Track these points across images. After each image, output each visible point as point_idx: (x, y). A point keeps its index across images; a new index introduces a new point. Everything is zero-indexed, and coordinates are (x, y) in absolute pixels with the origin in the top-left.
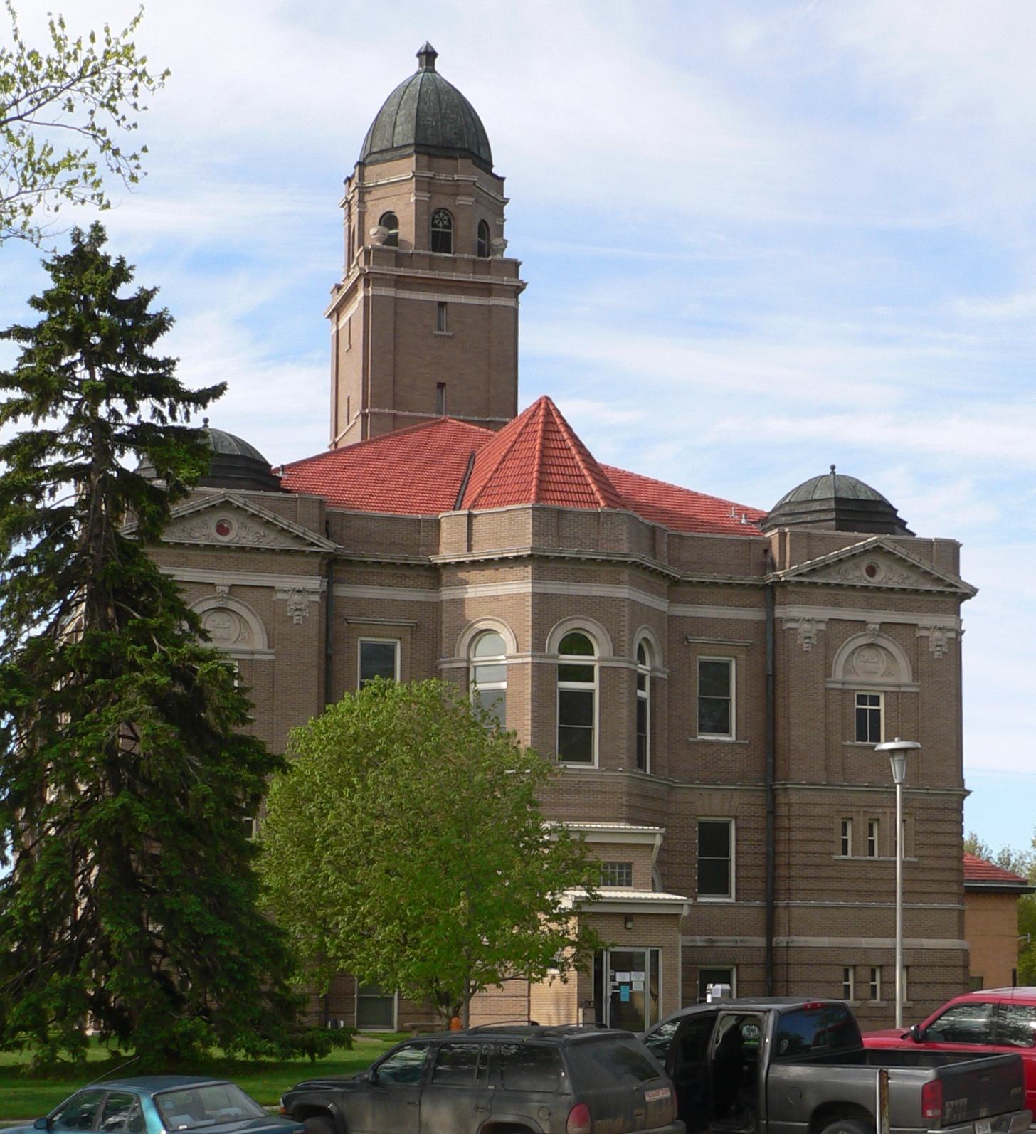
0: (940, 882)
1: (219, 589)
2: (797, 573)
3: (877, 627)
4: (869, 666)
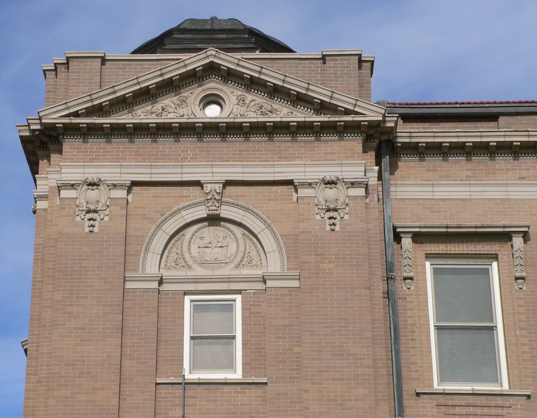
1: (208, 188)
2: (67, 112)
3: (218, 188)
4: (211, 254)
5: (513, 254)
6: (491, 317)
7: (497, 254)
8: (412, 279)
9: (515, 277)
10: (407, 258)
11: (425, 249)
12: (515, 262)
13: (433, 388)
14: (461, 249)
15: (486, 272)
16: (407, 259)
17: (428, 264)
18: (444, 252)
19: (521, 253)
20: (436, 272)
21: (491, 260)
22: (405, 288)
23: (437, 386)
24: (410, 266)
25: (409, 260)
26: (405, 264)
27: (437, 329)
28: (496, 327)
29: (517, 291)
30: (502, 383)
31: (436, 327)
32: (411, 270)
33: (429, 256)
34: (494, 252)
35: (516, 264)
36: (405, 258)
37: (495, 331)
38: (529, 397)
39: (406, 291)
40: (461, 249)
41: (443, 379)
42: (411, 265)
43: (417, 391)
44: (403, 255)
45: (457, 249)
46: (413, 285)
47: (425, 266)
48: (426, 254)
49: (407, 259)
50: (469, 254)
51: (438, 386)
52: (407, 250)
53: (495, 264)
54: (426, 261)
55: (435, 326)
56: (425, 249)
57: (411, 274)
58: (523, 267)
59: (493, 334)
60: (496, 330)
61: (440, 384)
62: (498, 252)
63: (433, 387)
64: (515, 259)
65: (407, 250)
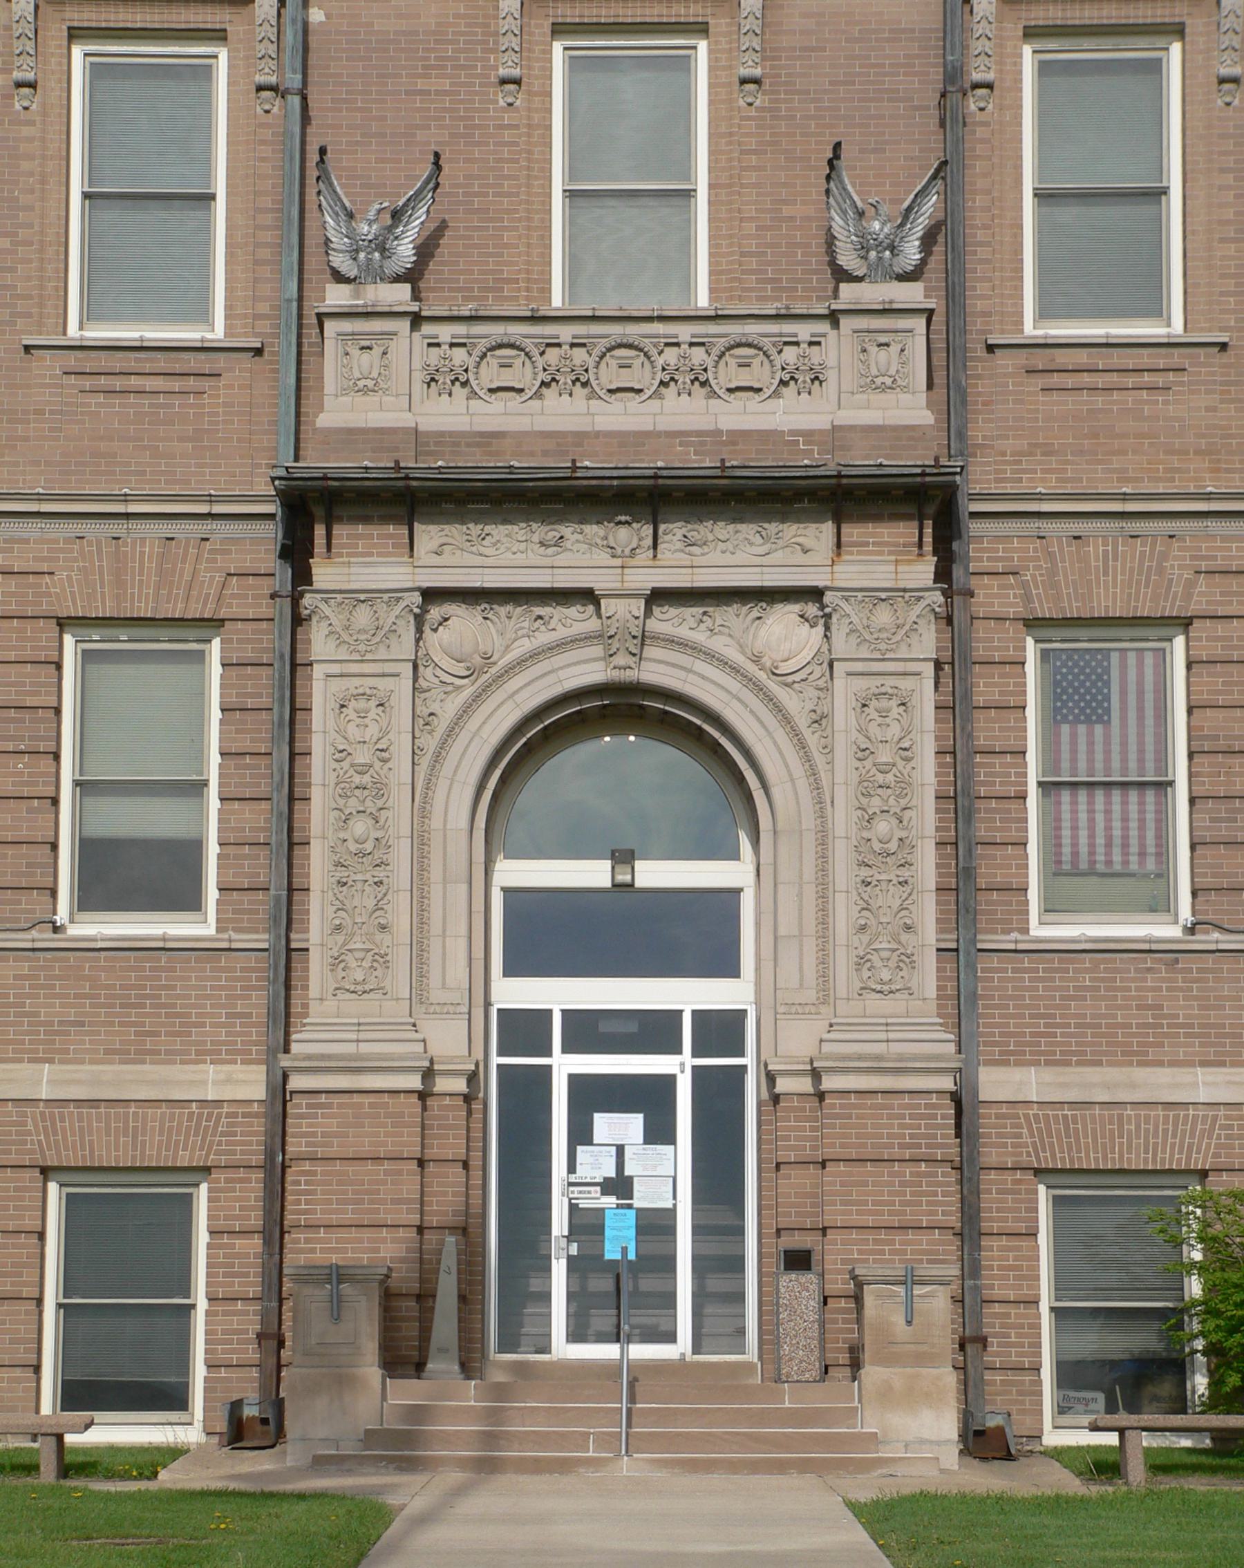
0: (1108, 828)
1: (607, 606)
5: (1219, 24)
6: (687, 171)
7: (225, 30)
8: (989, 86)
9: (1218, 77)
10: (23, 36)
11: (1023, 15)
12: (742, 42)
13: (1023, 333)
14: (1105, 13)
15: (1155, 68)
16: (983, 39)
17: (1027, 50)
18: (673, 20)
19: (757, 22)
20: (1045, 69)
21: (1169, 38)
22: (17, 106)
23: (1031, 329)
24: (989, 56)
25: (987, 42)
26: (976, 53)
27: (569, 197)
28: (695, 190)
29: (503, 110)
30: (1169, 318)
31: (567, 194)
32: (989, 65)
33: (1030, 33)
34: (218, 26)
35: (744, 48)
36: (978, 39)
37: (693, 200)
38: (1223, 346)
39: (18, 112)
40: (1087, 14)
41: (1045, 313)
42: (990, 53)
43: (990, 342)
44: (975, 29)
45: (1096, 14)
46: (991, 101)
47: (1021, 56)
48: (69, 28)
49: (983, 39)
50: (1138, 25)
51: (1034, 328)
52: (266, 22)
53: (1176, 48)
54: (1025, 43)
55: (565, 191)
56: (68, 15)
57: (990, 76)
58: (759, 55)
59: (1160, 203)
60: (695, 197)
61: (1038, 325)
62: (1184, 19)
63: (1022, 331)
64: (742, 36)
65: (266, 22)
